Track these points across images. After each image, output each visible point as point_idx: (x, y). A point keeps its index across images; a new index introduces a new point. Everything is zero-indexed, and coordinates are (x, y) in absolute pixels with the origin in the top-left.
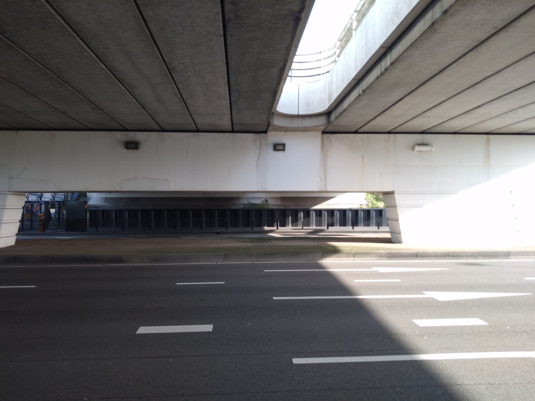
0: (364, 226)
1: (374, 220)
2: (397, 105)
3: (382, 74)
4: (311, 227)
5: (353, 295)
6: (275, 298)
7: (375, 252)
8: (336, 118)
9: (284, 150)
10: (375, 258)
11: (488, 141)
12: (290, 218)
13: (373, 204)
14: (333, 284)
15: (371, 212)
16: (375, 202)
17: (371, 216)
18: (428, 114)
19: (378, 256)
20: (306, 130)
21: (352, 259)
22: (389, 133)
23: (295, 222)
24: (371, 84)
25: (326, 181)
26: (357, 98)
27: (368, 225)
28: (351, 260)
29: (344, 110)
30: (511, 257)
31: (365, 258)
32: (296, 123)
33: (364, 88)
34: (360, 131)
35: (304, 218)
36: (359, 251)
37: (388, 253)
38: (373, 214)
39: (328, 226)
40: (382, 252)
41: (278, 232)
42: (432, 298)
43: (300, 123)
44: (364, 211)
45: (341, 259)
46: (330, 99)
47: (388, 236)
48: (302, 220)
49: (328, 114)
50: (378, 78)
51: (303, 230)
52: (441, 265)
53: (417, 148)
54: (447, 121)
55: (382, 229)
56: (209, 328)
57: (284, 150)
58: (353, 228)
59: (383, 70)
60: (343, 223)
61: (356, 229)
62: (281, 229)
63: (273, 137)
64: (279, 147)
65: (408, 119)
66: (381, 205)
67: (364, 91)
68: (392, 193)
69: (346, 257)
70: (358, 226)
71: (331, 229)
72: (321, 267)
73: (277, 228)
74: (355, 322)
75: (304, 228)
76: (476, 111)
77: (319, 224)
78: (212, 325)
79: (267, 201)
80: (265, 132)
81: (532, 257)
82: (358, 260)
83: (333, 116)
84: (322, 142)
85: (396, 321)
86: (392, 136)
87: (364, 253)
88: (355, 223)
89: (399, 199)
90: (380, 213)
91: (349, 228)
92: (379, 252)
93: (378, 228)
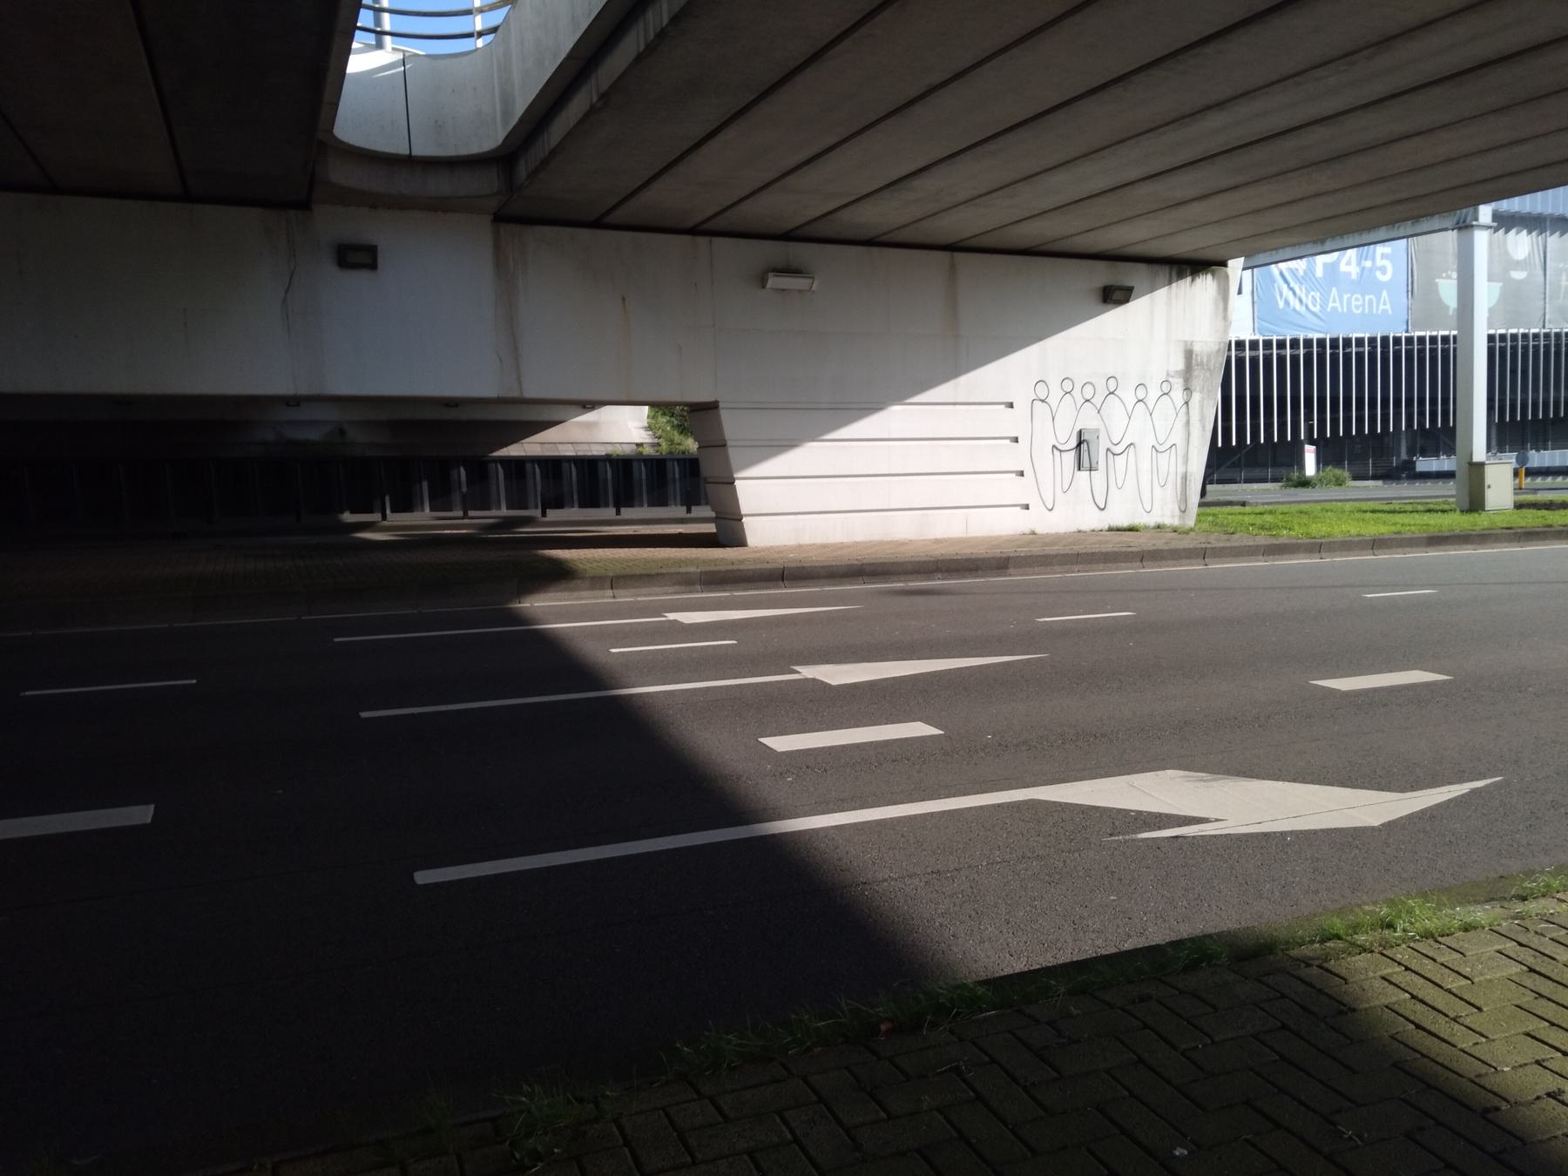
0: (651, 504)
1: (675, 489)
2: (704, 149)
3: (651, 48)
4: (494, 513)
5: (606, 689)
6: (364, 715)
7: (673, 570)
8: (533, 174)
9: (373, 266)
10: (671, 589)
11: (953, 267)
12: (425, 484)
13: (672, 442)
14: (558, 663)
15: (669, 464)
16: (677, 437)
17: (670, 476)
18: (791, 180)
19: (679, 583)
20: (438, 206)
21: (610, 592)
22: (694, 231)
23: (441, 501)
24: (621, 77)
25: (518, 368)
26: (587, 115)
27: (662, 502)
28: (605, 597)
29: (553, 153)
30: (1011, 571)
31: (644, 591)
32: (439, 185)
33: (604, 87)
34: (613, 218)
35: (470, 482)
36: (628, 571)
37: (706, 573)
38: (675, 471)
39: (545, 507)
40: (692, 569)
41: (385, 527)
42: (814, 680)
43: (419, 184)
44: (648, 461)
45: (576, 594)
46: (506, 113)
47: (711, 528)
48: (464, 489)
49: (504, 158)
50: (639, 58)
51: (466, 521)
52: (839, 598)
53: (773, 281)
54: (845, 206)
55: (698, 511)
56: (142, 814)
57: (373, 266)
58: (618, 513)
59: (651, 36)
60: (591, 499)
61: (627, 513)
62: (395, 519)
63: (334, 224)
64: (357, 257)
65: (743, 194)
66: (691, 445)
67: (604, 96)
68: (713, 407)
69: (592, 588)
70: (632, 506)
71: (553, 515)
72: (518, 619)
73: (384, 517)
74: (625, 758)
75: (471, 513)
76: (916, 182)
77: (518, 501)
78: (152, 807)
79: (342, 432)
80: (305, 205)
81: (1057, 568)
82: (625, 597)
83: (522, 170)
84: (497, 246)
85: (715, 745)
86: (702, 241)
87: (641, 577)
88: (625, 498)
89: (732, 425)
90: (691, 466)
91: (609, 513)
92: (682, 570)
93: (689, 511)
